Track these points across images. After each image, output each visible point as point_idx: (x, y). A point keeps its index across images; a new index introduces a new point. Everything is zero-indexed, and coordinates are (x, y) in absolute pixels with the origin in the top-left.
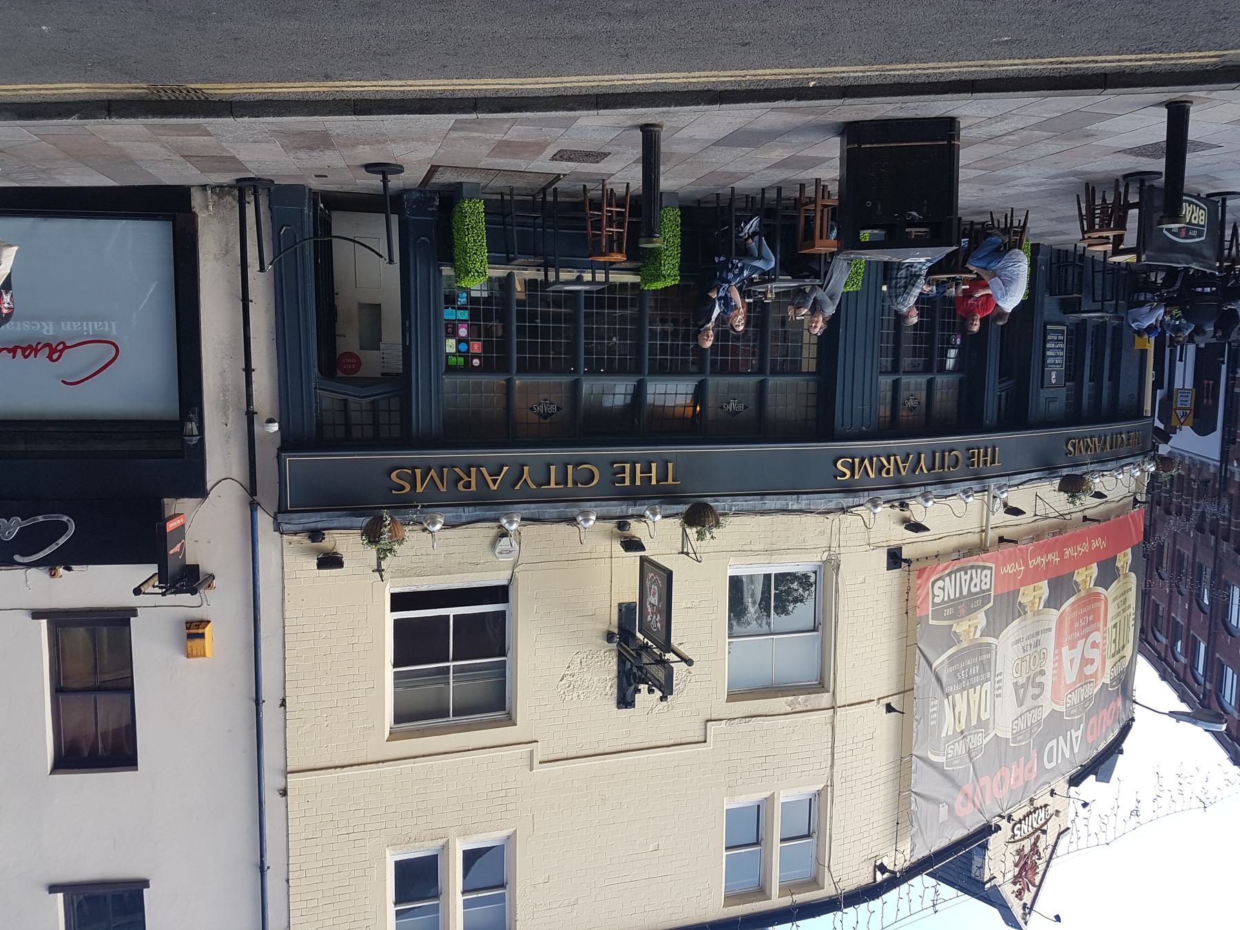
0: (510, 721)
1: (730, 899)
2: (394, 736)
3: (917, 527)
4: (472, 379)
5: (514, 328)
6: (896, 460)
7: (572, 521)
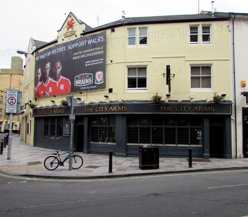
0: (190, 65)
1: (147, 28)
2: (212, 64)
3: (107, 97)
4: (197, 127)
5: (103, 143)
6: (113, 110)
7: (123, 101)
